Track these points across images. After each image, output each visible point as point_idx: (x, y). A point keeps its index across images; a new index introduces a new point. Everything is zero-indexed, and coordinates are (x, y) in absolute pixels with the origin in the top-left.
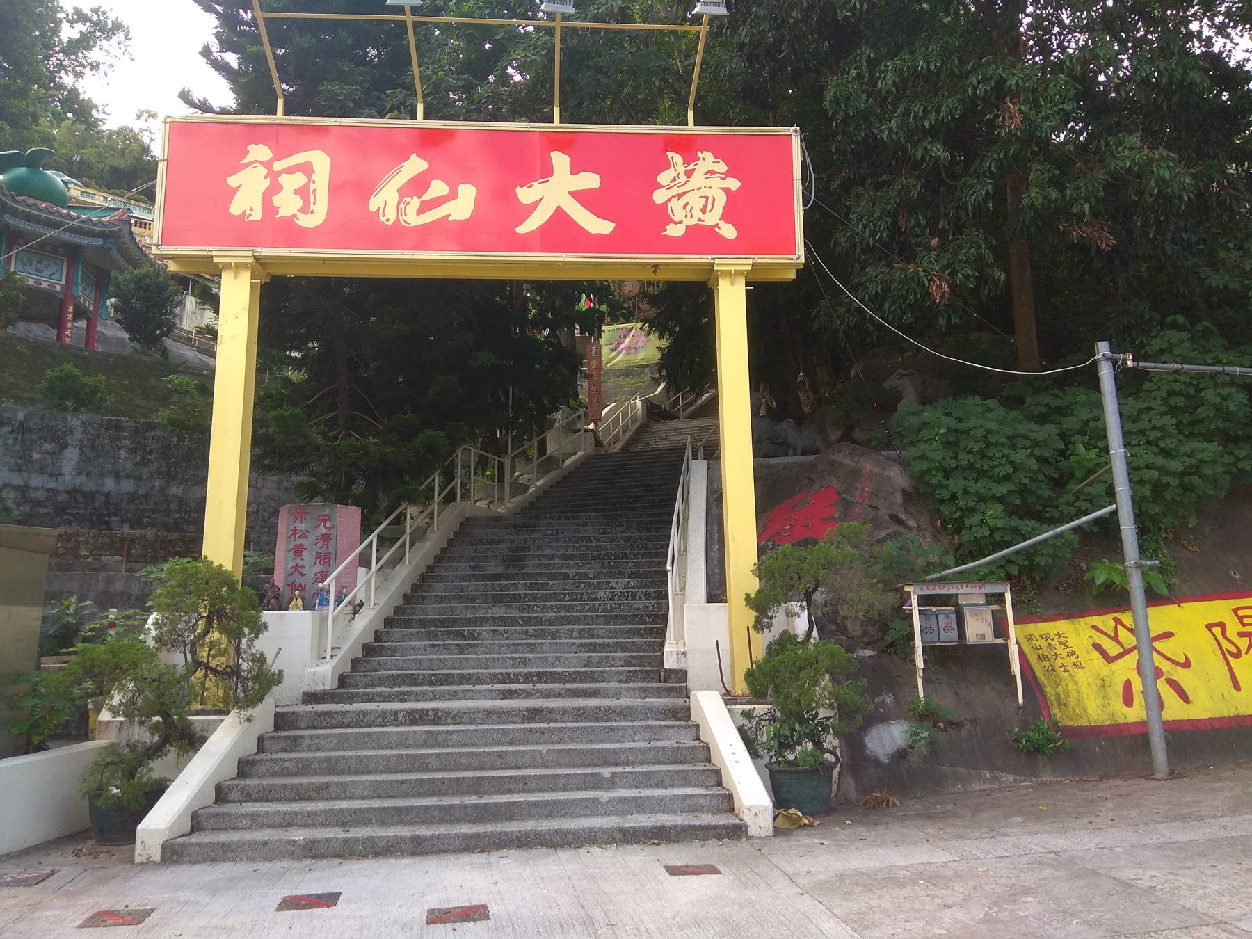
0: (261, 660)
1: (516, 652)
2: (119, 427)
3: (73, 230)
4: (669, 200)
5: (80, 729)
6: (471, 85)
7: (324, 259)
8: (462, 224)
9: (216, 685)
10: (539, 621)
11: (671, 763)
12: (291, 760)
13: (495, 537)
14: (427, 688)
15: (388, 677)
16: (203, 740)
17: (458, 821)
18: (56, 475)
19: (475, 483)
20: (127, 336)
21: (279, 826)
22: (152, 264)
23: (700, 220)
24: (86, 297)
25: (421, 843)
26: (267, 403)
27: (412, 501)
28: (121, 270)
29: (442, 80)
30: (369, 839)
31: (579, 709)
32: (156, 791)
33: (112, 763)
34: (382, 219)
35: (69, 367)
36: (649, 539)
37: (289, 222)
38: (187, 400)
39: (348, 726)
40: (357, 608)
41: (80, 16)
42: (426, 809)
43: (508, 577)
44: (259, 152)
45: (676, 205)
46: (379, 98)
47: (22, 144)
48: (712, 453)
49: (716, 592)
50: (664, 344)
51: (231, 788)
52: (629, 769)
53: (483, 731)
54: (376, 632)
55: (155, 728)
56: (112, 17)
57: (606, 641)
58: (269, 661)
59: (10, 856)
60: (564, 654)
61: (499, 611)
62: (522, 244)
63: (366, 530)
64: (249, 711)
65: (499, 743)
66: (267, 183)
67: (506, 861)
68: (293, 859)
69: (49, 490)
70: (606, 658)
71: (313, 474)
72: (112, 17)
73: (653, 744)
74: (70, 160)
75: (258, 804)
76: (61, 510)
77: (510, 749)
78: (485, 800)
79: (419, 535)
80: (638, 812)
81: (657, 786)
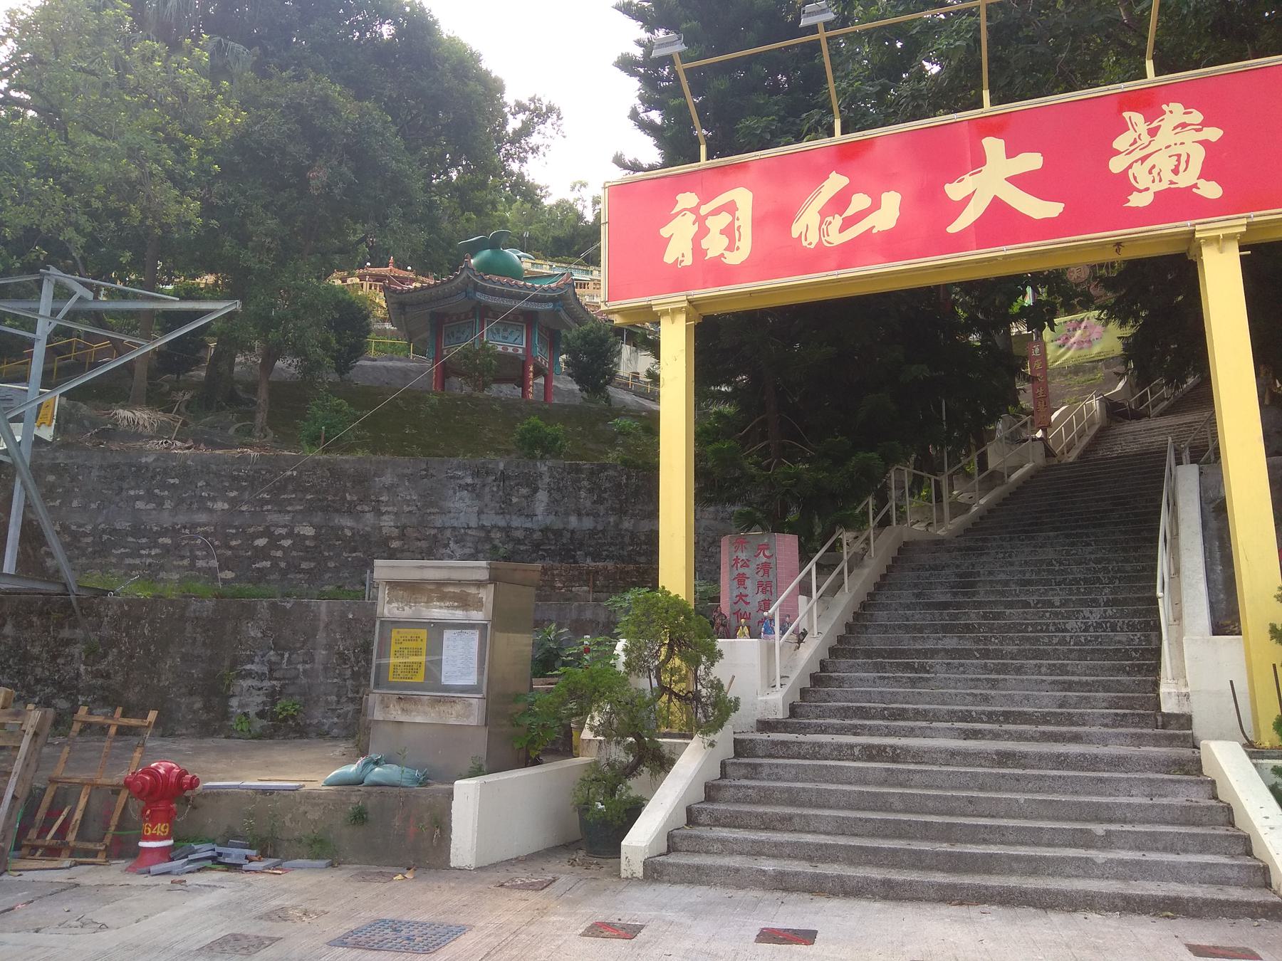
0: (717, 686)
1: (976, 688)
2: (578, 470)
3: (535, 299)
4: (1130, 166)
5: (565, 746)
6: (889, 88)
7: (751, 293)
8: (888, 234)
9: (680, 709)
10: (998, 654)
11: (1181, 824)
12: (753, 788)
13: (938, 562)
14: (881, 722)
15: (839, 709)
16: (672, 762)
17: (931, 868)
18: (531, 516)
19: (910, 504)
20: (576, 387)
21: (748, 854)
22: (594, 320)
23: (1172, 182)
24: (542, 357)
25: (892, 888)
26: (705, 436)
27: (848, 527)
28: (569, 329)
29: (859, 90)
30: (839, 877)
31: (1059, 755)
32: (633, 811)
33: (596, 780)
35: (534, 420)
36: (1126, 560)
37: (717, 263)
38: (631, 441)
39: (805, 758)
40: (801, 636)
41: (521, 108)
42: (894, 851)
43: (958, 606)
44: (687, 200)
46: (794, 124)
47: (483, 230)
48: (1206, 453)
49: (1225, 620)
50: (1128, 331)
51: (700, 811)
52: (1127, 828)
53: (949, 774)
54: (822, 662)
55: (629, 748)
56: (545, 102)
57: (1084, 678)
58: (726, 688)
59: (518, 861)
60: (1033, 691)
61: (951, 642)
62: (958, 243)
63: (804, 557)
64: (712, 737)
65: (967, 788)
67: (989, 917)
68: (765, 889)
69: (526, 529)
70: (1086, 698)
71: (750, 504)
72: (545, 102)
73: (1156, 801)
74: (521, 238)
75: (726, 830)
76: (537, 546)
77: (982, 795)
78: (958, 848)
79: (857, 561)
80: (1144, 878)
81: (1165, 850)
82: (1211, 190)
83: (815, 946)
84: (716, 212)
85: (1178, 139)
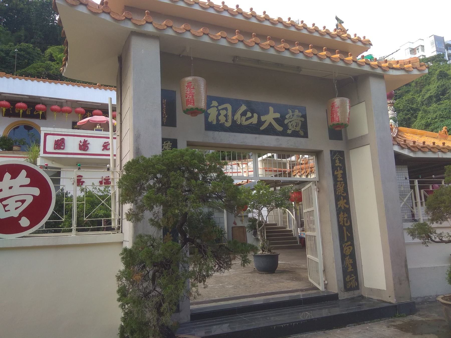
45: (290, 124)
84: (223, 109)
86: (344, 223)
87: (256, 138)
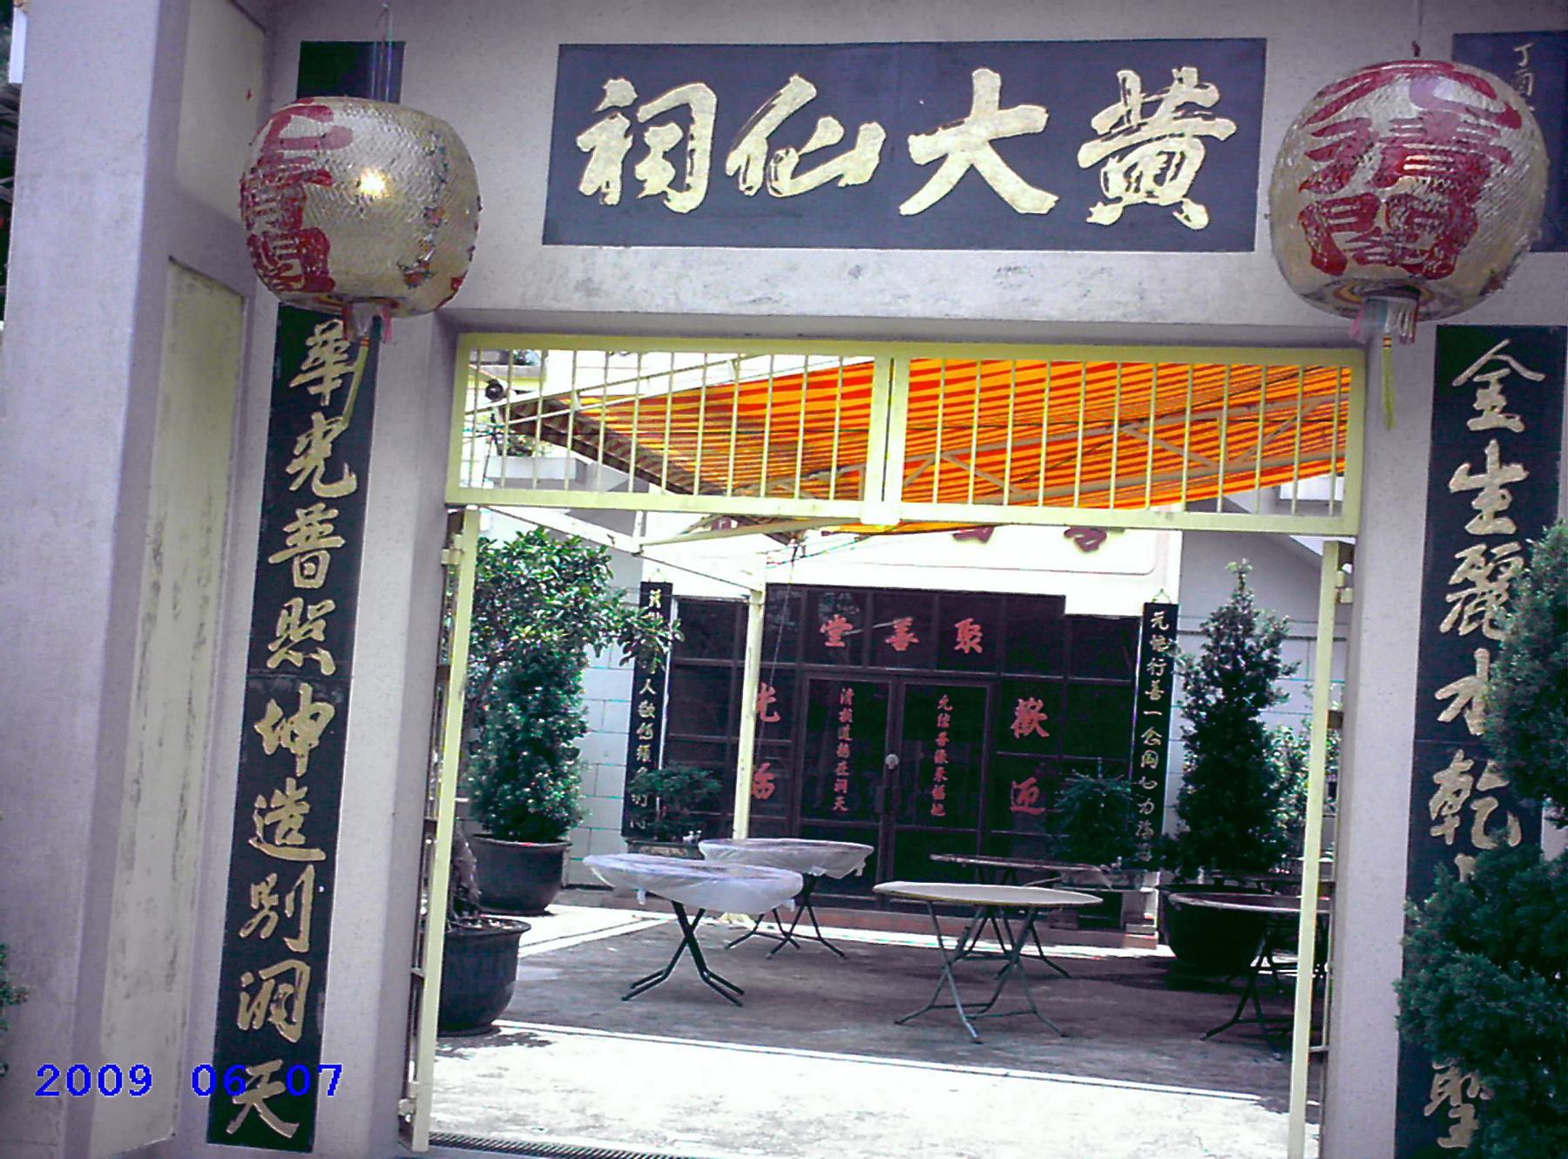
8: (1469, 836)
34: (742, 187)
45: (1114, 169)
66: (629, 143)
82: (1197, 216)
83: (858, 149)
85: (1176, 126)
86: (1463, 833)
87: (857, 272)
